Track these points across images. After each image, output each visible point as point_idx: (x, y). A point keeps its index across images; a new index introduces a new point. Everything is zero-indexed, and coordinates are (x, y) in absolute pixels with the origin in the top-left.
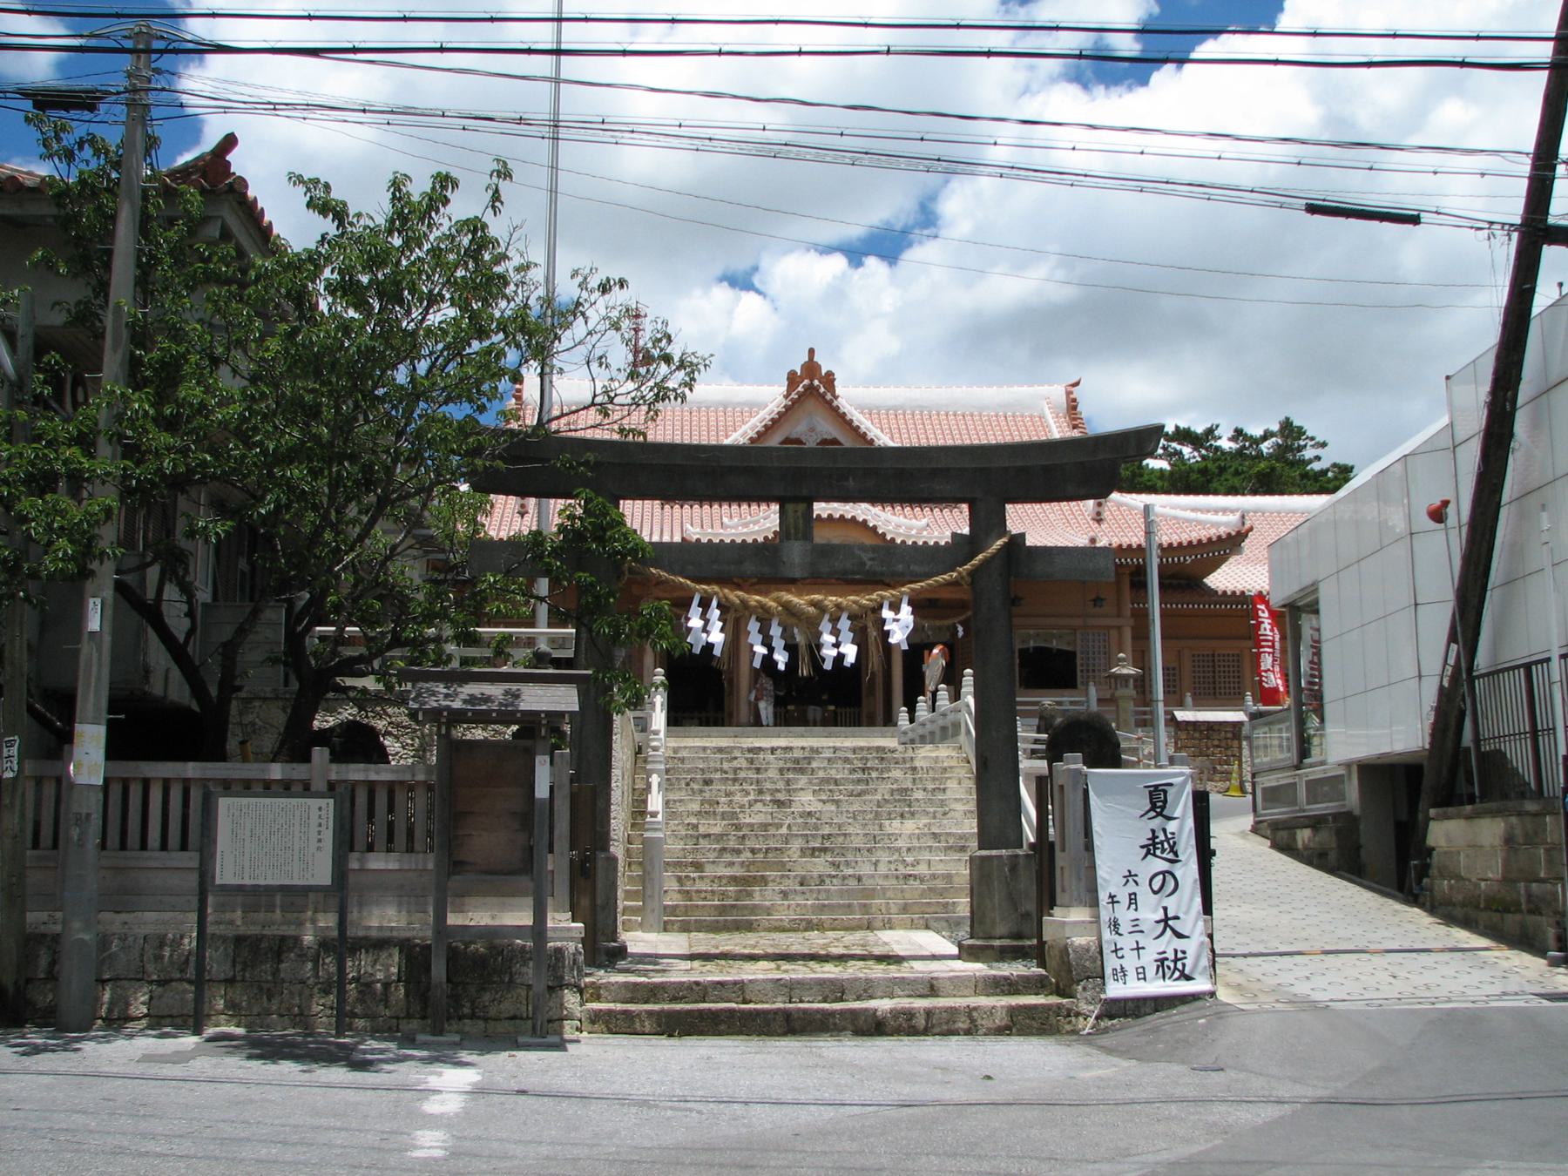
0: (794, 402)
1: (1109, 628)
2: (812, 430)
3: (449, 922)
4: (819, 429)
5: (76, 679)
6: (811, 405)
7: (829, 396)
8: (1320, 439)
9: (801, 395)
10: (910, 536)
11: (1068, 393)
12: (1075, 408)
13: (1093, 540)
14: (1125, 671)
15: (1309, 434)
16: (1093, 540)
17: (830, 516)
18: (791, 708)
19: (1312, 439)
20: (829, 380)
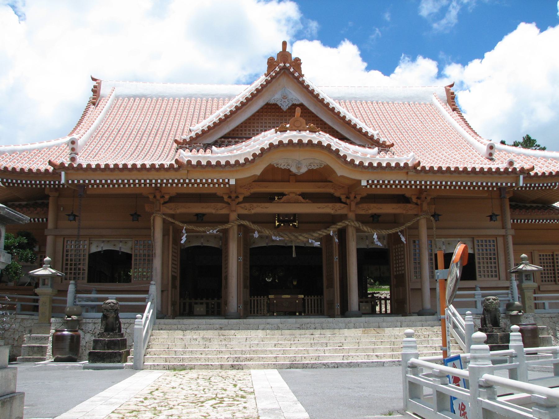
0: (273, 78)
1: (496, 237)
2: (285, 97)
3: (319, 243)
4: (290, 97)
5: (221, 263)
6: (284, 81)
7: (296, 74)
8: (542, 146)
9: (277, 73)
10: (366, 159)
11: (447, 91)
12: (453, 98)
13: (511, 163)
14: (529, 268)
15: (537, 143)
16: (511, 163)
17: (300, 141)
18: (271, 296)
19: (539, 146)
20: (297, 63)
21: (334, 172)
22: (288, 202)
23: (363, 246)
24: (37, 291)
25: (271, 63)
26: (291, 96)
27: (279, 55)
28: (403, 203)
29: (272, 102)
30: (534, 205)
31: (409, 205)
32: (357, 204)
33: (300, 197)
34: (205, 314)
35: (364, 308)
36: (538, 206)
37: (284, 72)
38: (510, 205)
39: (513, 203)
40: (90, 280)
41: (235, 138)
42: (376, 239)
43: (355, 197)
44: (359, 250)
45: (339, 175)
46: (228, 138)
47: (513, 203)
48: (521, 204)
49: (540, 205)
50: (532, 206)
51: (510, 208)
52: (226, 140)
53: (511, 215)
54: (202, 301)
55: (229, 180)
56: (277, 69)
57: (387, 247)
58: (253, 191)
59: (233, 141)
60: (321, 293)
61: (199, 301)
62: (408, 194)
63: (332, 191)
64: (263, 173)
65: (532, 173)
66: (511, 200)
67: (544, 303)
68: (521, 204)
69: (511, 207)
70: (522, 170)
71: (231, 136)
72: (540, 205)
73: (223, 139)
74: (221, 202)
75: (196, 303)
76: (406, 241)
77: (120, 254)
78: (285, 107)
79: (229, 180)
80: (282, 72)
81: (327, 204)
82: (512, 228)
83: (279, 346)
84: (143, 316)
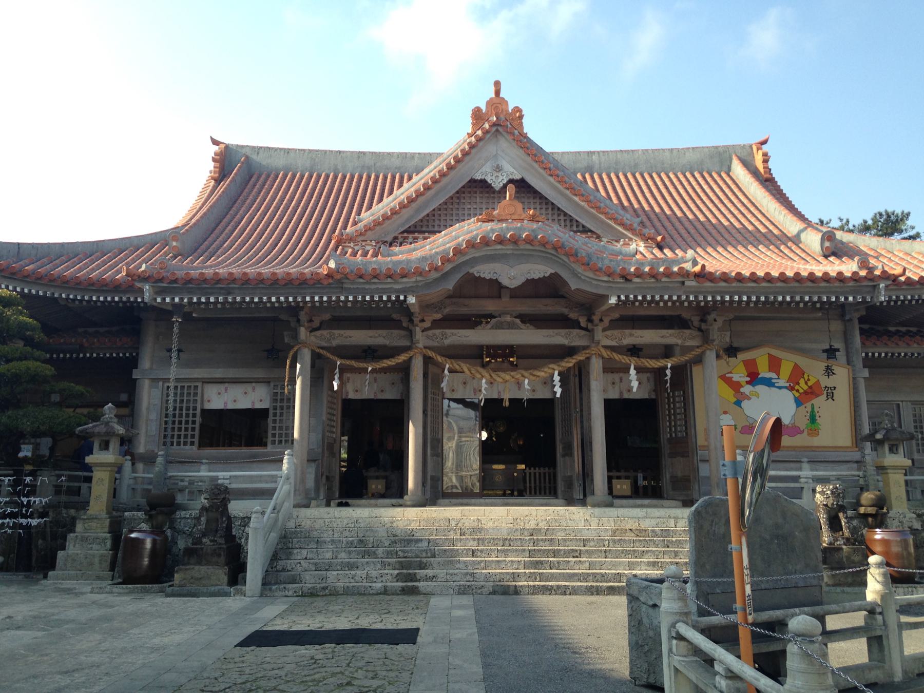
0: (479, 140)
21: (565, 283)
22: (499, 326)
23: (614, 395)
24: (89, 459)
25: (477, 115)
26: (502, 167)
27: (490, 103)
28: (679, 328)
29: (478, 177)
30: (904, 329)
31: (687, 332)
32: (604, 330)
33: (518, 321)
34: (629, 493)
35: (619, 487)
36: (909, 331)
37: (497, 130)
38: (861, 329)
39: (866, 327)
40: (201, 446)
41: (424, 232)
42: (634, 385)
43: (601, 320)
44: (608, 403)
45: (573, 287)
46: (413, 232)
47: (866, 327)
48: (880, 328)
49: (914, 329)
50: (898, 331)
51: (861, 334)
52: (411, 236)
53: (863, 344)
54: (618, 474)
55: (405, 297)
56: (487, 126)
57: (653, 397)
58: (446, 311)
59: (421, 236)
60: (552, 464)
61: (622, 474)
62: (685, 315)
63: (565, 311)
64: (455, 288)
65: (903, 279)
66: (861, 320)
67: (80, 487)
68: (880, 328)
69: (862, 332)
70: (885, 275)
71: (418, 229)
72: (914, 329)
73: (405, 235)
74: (399, 329)
75: (619, 478)
76: (638, 388)
77: (507, 404)
78: (497, 186)
79: (405, 297)
80: (494, 129)
81: (556, 331)
82: (864, 367)
83: (541, 543)
84: (464, 496)
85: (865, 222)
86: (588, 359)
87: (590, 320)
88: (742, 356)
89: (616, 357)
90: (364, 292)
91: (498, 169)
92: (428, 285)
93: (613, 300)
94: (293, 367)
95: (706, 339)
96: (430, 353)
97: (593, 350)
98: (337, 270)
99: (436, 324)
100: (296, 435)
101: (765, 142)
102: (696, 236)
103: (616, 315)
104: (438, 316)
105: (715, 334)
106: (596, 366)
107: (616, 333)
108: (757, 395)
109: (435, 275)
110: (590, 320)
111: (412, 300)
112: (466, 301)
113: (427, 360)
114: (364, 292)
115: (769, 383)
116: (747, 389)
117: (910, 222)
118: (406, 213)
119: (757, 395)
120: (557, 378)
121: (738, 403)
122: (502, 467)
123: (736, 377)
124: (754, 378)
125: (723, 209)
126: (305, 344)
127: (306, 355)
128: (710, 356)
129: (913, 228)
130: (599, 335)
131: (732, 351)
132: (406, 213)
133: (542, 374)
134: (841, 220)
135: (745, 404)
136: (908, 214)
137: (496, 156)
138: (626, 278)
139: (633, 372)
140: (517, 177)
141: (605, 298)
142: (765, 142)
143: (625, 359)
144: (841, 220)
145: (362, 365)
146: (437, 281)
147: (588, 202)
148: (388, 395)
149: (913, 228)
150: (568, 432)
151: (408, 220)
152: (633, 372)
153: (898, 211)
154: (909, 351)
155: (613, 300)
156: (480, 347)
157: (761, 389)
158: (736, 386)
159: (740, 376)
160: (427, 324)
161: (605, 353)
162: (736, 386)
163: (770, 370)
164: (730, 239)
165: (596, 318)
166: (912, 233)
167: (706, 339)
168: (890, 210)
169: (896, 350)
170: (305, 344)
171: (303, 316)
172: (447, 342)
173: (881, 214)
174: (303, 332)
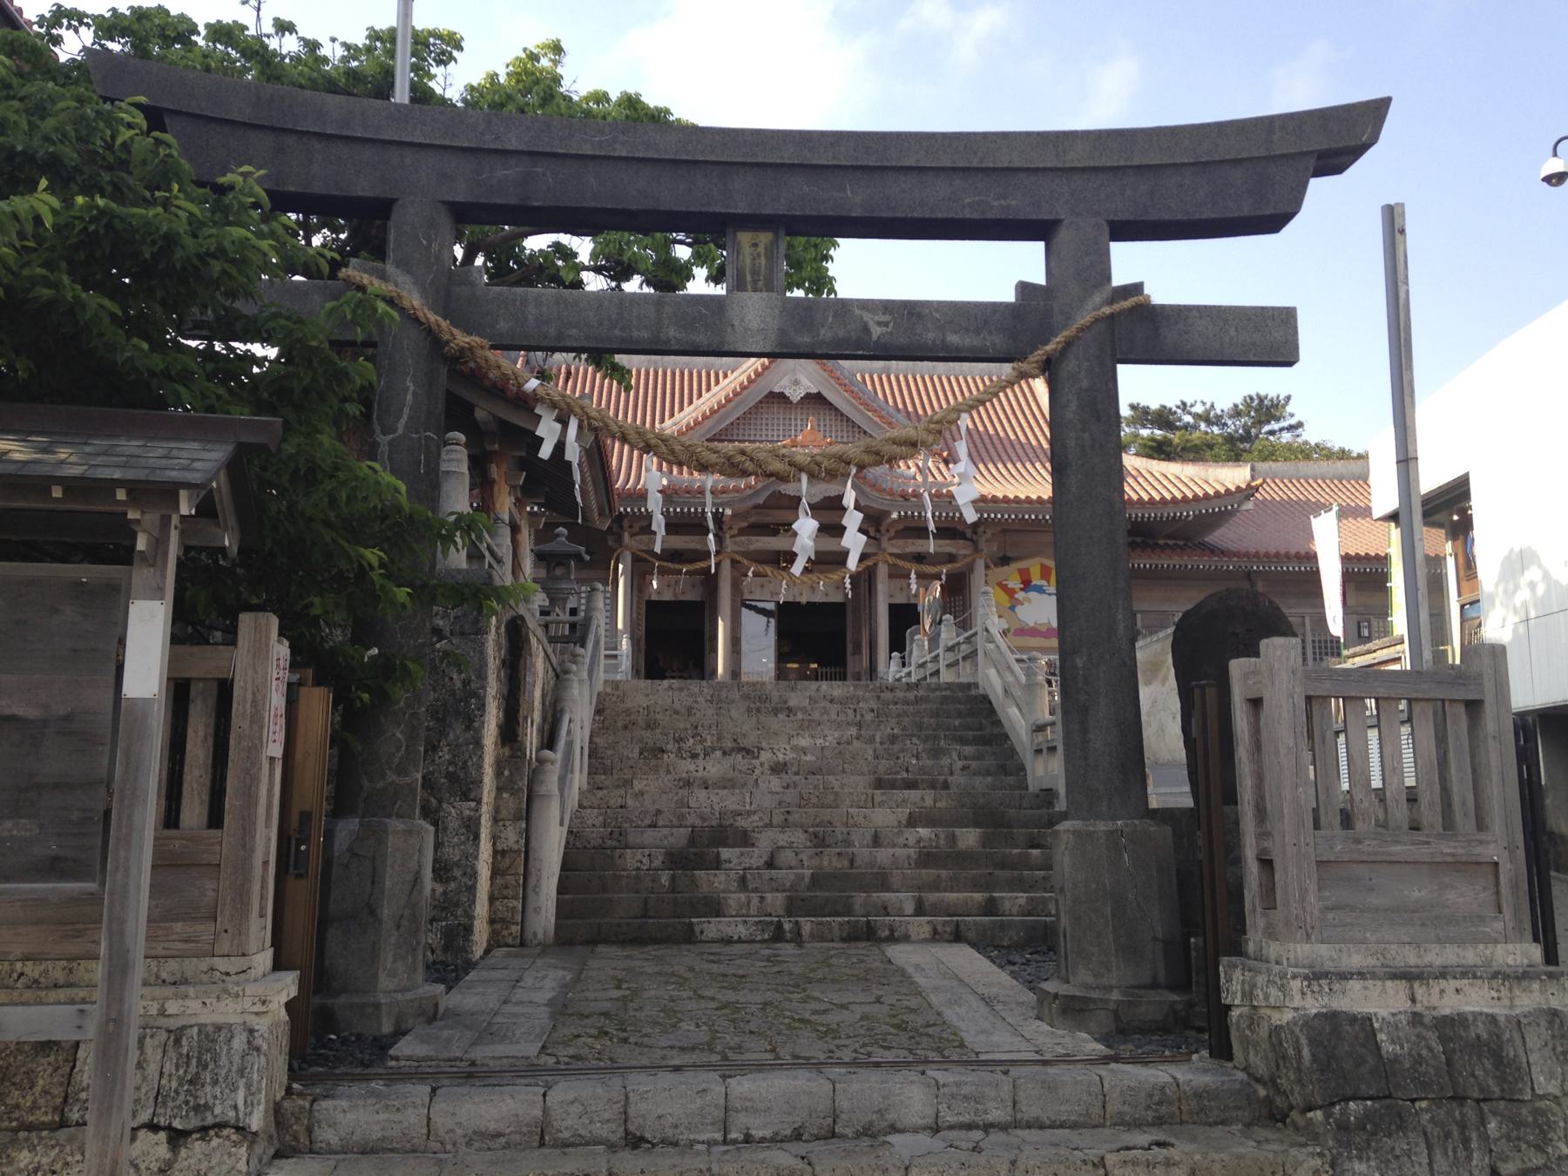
30: (1171, 542)
58: (753, 520)
68: (1151, 542)
85: (1236, 406)
86: (875, 564)
87: (878, 531)
88: (1015, 566)
89: (901, 563)
90: (689, 505)
91: (796, 382)
92: (743, 500)
93: (895, 516)
94: (616, 568)
95: (977, 550)
96: (738, 558)
97: (880, 557)
98: (669, 486)
99: (742, 532)
100: (620, 626)
101: (1246, 176)
102: (982, 451)
103: (901, 527)
104: (744, 524)
105: (982, 545)
106: (882, 571)
107: (901, 542)
108: (1029, 601)
109: (749, 492)
110: (878, 531)
111: (729, 512)
112: (771, 512)
113: (734, 562)
114: (689, 505)
115: (1040, 590)
116: (1020, 595)
117: (1289, 409)
118: (709, 424)
119: (1029, 601)
120: (848, 581)
121: (1012, 608)
122: (795, 666)
123: (1011, 585)
124: (1027, 585)
125: (1013, 421)
126: (627, 548)
127: (628, 556)
128: (980, 565)
129: (1292, 415)
130: (885, 543)
131: (1005, 561)
132: (709, 424)
133: (835, 577)
134: (1204, 403)
135: (1018, 609)
136: (1288, 398)
137: (794, 371)
138: (905, 497)
139: (913, 576)
140: (815, 391)
141: (889, 513)
142: (1246, 176)
143: (907, 565)
144: (1204, 403)
145: (677, 566)
146: (750, 496)
147: (881, 417)
148: (689, 597)
149: (1292, 415)
150: (858, 631)
151: (709, 430)
152: (913, 576)
153: (1272, 394)
154: (1172, 563)
155: (895, 516)
156: (778, 553)
157: (1033, 595)
158: (1010, 593)
159: (1014, 583)
160: (735, 532)
161: (890, 560)
162: (1010, 593)
163: (1042, 578)
164: (1013, 455)
165: (883, 529)
166: (1293, 421)
167: (977, 550)
168: (1262, 393)
169: (1159, 562)
170: (627, 548)
171: (626, 523)
172: (752, 547)
173: (1251, 398)
174: (626, 537)
